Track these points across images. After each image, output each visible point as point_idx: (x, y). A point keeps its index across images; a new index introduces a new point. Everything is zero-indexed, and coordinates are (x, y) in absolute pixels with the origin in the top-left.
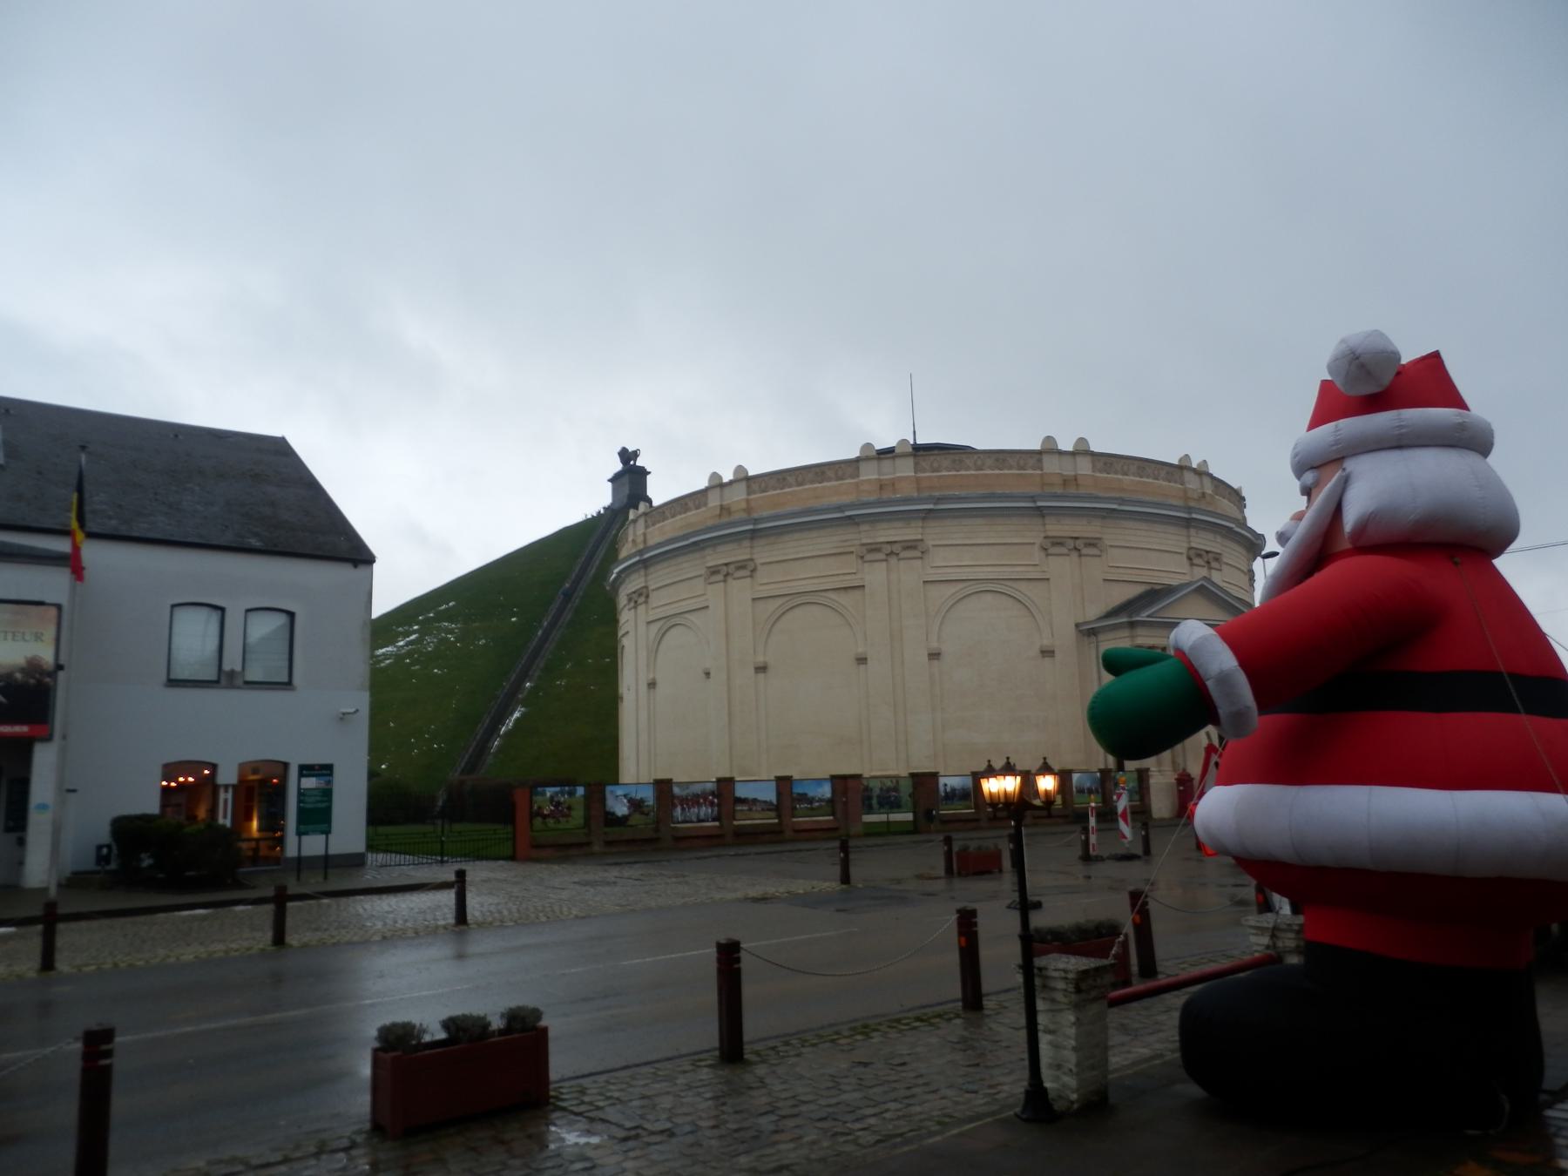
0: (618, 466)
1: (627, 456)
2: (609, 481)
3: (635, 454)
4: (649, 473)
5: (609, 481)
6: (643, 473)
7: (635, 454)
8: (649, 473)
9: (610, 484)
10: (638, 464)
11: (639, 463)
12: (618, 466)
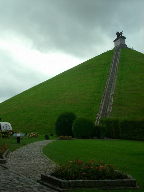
0: (116, 37)
1: (119, 35)
2: (114, 41)
3: (122, 33)
4: (126, 38)
5: (114, 41)
6: (124, 38)
7: (122, 33)
8: (126, 38)
9: (114, 42)
11: (123, 35)
12: (116, 37)
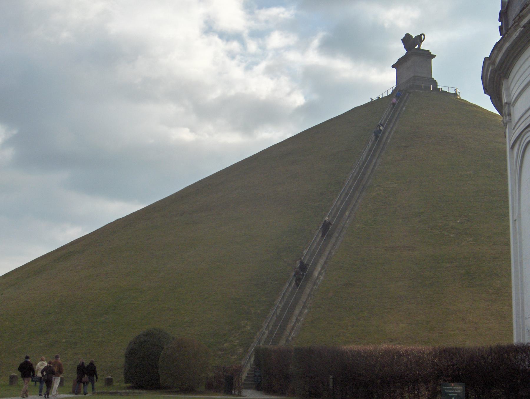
0: (403, 52)
2: (393, 66)
3: (420, 39)
4: (434, 56)
6: (428, 56)
7: (420, 39)
8: (434, 56)
9: (395, 69)
10: (422, 48)
12: (403, 52)
